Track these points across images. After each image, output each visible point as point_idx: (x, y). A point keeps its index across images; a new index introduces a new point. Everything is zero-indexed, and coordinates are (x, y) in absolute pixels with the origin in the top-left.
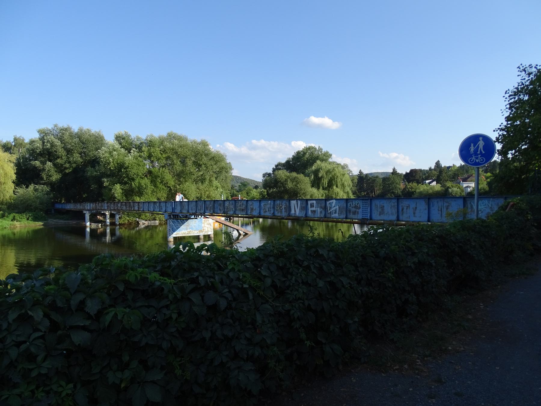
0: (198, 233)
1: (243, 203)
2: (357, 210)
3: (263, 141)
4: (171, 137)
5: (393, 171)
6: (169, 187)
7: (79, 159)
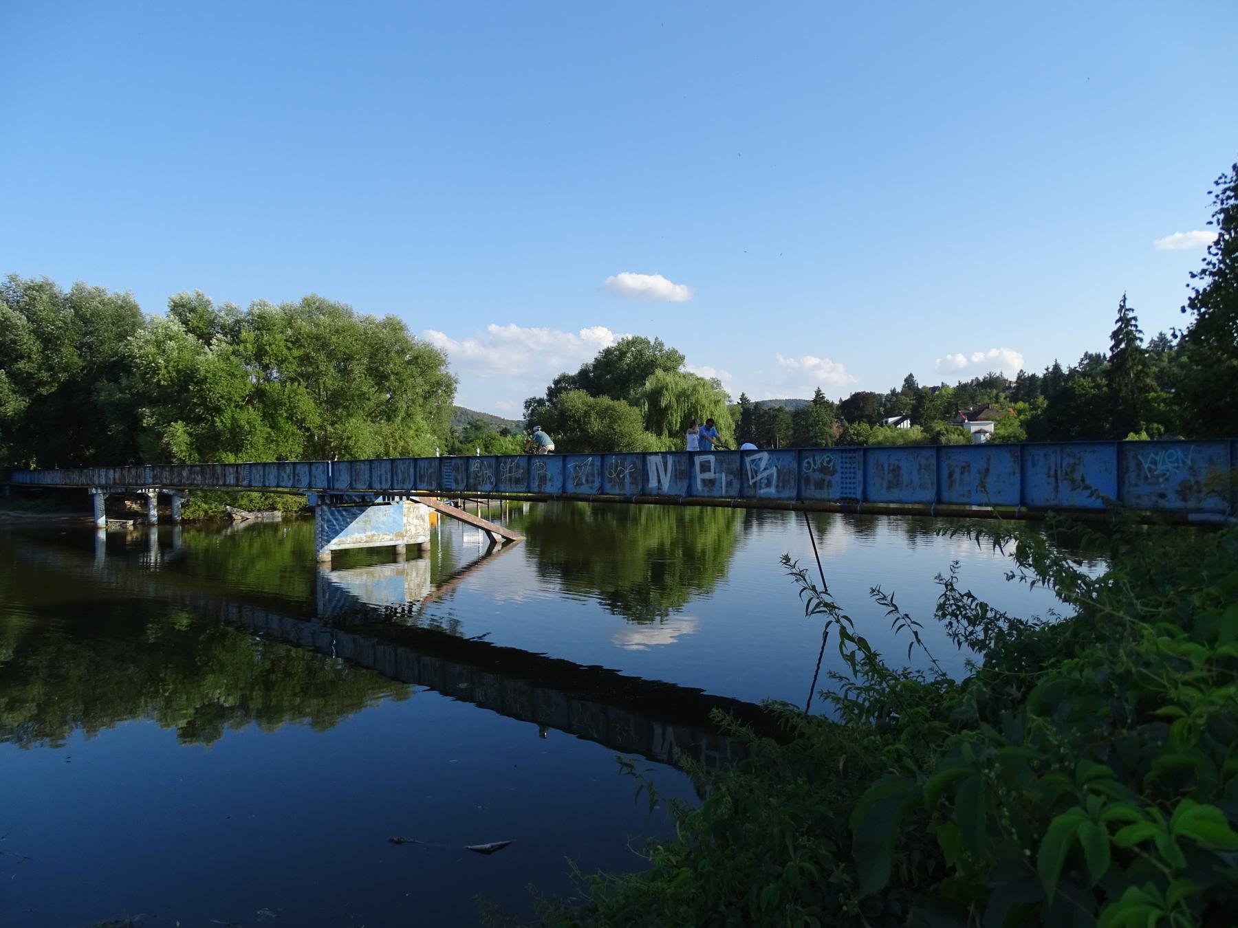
0: (391, 540)
1: (517, 463)
2: (828, 478)
3: (514, 329)
4: (312, 307)
5: (816, 396)
6: (308, 429)
7: (76, 359)
